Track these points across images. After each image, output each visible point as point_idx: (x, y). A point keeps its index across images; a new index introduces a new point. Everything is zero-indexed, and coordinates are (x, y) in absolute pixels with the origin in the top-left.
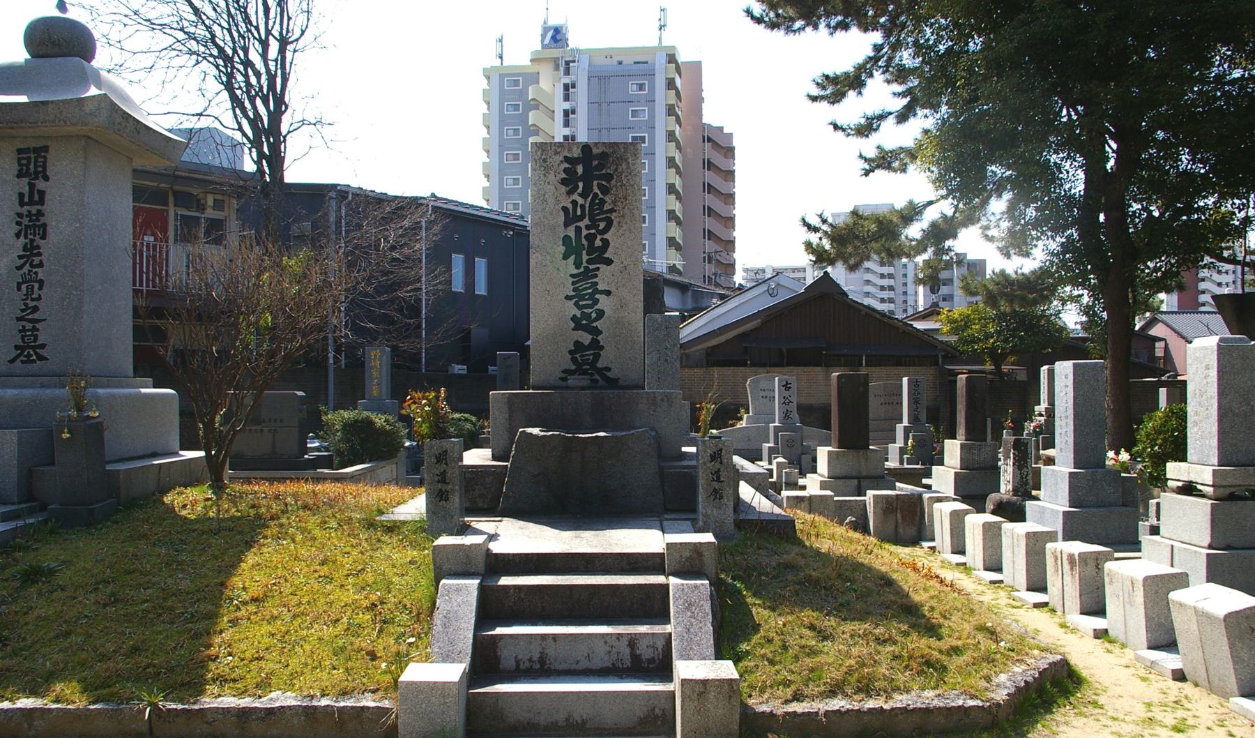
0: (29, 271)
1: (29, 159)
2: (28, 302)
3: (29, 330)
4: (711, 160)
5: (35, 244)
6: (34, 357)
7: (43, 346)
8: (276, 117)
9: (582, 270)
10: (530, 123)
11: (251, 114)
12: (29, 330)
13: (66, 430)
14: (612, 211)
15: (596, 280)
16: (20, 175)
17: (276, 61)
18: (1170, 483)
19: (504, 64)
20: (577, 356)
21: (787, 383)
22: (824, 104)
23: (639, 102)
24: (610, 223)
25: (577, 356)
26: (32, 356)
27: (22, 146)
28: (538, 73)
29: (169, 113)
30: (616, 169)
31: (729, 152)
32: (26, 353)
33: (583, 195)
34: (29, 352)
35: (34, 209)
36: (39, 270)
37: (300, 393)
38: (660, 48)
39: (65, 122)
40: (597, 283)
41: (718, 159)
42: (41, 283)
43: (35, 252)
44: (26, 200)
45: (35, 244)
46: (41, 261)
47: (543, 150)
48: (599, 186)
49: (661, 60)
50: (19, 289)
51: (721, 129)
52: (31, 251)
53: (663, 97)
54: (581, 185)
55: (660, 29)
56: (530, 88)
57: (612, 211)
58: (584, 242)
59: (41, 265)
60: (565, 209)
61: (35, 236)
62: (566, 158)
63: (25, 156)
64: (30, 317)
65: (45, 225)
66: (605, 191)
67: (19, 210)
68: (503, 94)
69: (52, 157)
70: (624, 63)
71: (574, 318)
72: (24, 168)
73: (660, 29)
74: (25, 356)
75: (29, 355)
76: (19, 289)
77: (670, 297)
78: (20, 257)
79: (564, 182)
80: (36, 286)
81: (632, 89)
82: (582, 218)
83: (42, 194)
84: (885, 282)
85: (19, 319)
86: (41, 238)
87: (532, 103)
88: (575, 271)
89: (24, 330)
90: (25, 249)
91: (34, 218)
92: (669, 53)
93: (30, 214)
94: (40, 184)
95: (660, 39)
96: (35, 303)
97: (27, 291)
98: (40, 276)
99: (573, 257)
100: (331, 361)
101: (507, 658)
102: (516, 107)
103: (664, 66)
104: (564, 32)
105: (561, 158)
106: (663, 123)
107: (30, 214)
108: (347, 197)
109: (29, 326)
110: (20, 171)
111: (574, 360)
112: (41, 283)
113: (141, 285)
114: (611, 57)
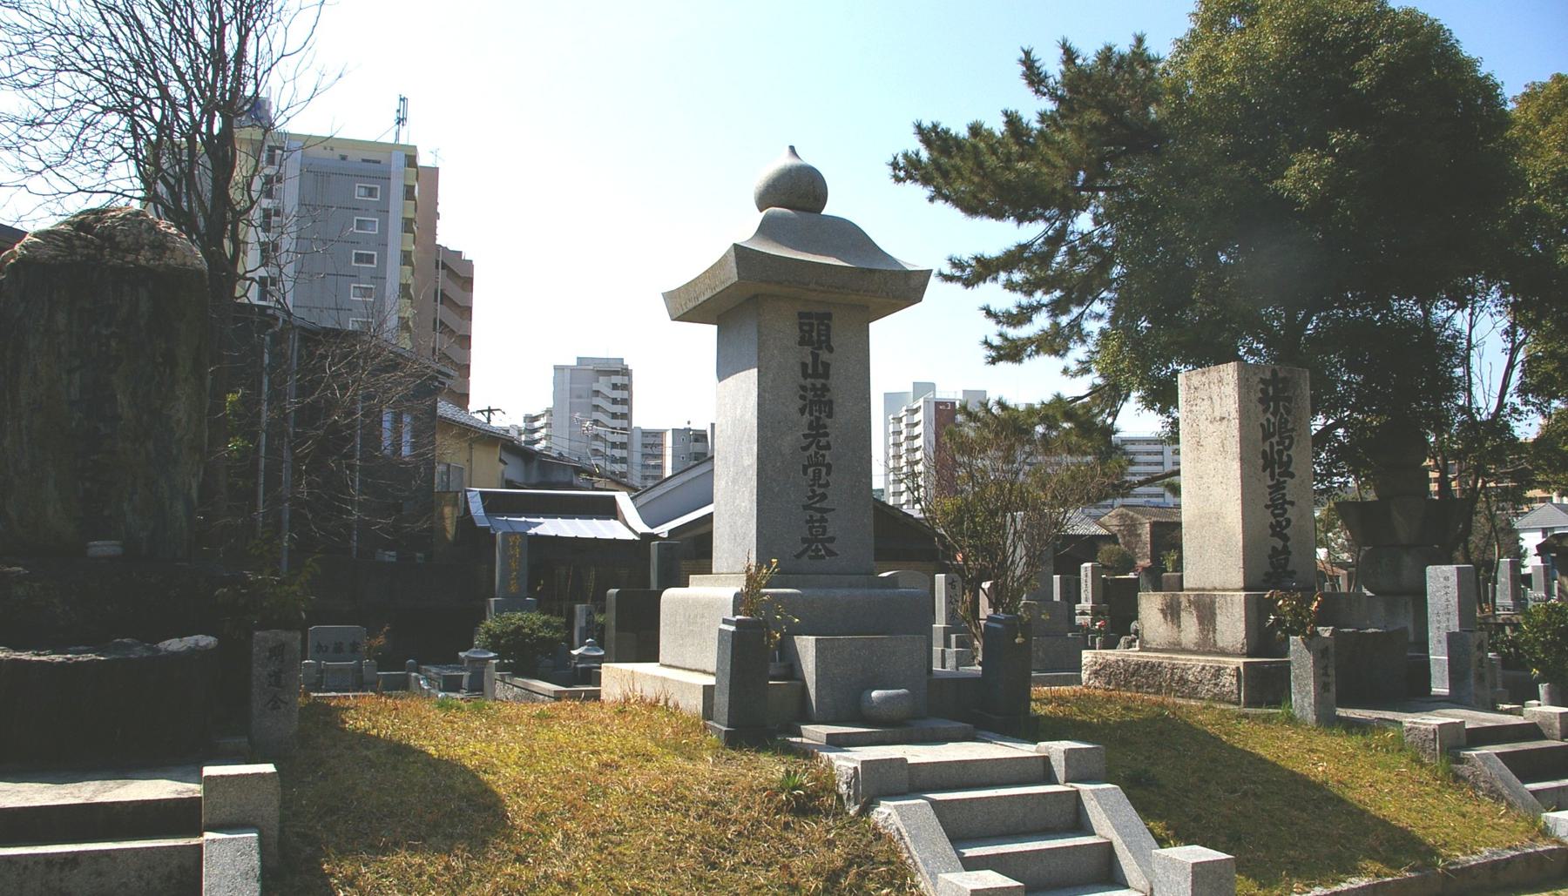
0: (816, 453)
1: (811, 325)
2: (815, 488)
3: (816, 521)
4: (447, 293)
5: (821, 423)
6: (823, 552)
7: (832, 540)
9: (1275, 482)
12: (816, 521)
13: (1019, 635)
14: (1293, 430)
15: (1284, 491)
16: (802, 343)
20: (1274, 560)
21: (954, 581)
22: (958, 286)
23: (367, 210)
25: (1274, 560)
26: (820, 550)
27: (806, 310)
30: (1294, 393)
31: (467, 283)
32: (813, 547)
34: (817, 546)
35: (819, 383)
36: (827, 453)
38: (395, 147)
39: (887, 293)
40: (1284, 495)
41: (454, 291)
42: (829, 467)
43: (821, 431)
44: (810, 371)
45: (821, 423)
46: (828, 442)
47: (1246, 370)
48: (1285, 407)
49: (398, 162)
50: (805, 473)
52: (817, 431)
53: (398, 208)
54: (1272, 404)
57: (1293, 430)
58: (1276, 457)
59: (828, 447)
60: (1262, 425)
61: (820, 413)
62: (1261, 379)
63: (807, 321)
64: (818, 505)
65: (831, 402)
66: (1288, 412)
67: (802, 381)
70: (349, 159)
72: (807, 335)
73: (399, 123)
74: (813, 551)
75: (818, 550)
76: (805, 473)
78: (805, 436)
79: (1261, 401)
80: (824, 470)
81: (359, 193)
82: (1273, 435)
83: (827, 366)
84: (618, 453)
85: (806, 507)
86: (827, 416)
88: (1271, 483)
89: (811, 521)
90: (810, 427)
91: (819, 392)
93: (814, 388)
94: (824, 356)
95: (397, 134)
96: (822, 490)
97: (814, 476)
98: (828, 460)
99: (1269, 470)
103: (402, 170)
104: (267, 108)
105: (1258, 380)
106: (397, 242)
107: (814, 388)
109: (817, 516)
110: (802, 338)
111: (1272, 563)
112: (829, 467)
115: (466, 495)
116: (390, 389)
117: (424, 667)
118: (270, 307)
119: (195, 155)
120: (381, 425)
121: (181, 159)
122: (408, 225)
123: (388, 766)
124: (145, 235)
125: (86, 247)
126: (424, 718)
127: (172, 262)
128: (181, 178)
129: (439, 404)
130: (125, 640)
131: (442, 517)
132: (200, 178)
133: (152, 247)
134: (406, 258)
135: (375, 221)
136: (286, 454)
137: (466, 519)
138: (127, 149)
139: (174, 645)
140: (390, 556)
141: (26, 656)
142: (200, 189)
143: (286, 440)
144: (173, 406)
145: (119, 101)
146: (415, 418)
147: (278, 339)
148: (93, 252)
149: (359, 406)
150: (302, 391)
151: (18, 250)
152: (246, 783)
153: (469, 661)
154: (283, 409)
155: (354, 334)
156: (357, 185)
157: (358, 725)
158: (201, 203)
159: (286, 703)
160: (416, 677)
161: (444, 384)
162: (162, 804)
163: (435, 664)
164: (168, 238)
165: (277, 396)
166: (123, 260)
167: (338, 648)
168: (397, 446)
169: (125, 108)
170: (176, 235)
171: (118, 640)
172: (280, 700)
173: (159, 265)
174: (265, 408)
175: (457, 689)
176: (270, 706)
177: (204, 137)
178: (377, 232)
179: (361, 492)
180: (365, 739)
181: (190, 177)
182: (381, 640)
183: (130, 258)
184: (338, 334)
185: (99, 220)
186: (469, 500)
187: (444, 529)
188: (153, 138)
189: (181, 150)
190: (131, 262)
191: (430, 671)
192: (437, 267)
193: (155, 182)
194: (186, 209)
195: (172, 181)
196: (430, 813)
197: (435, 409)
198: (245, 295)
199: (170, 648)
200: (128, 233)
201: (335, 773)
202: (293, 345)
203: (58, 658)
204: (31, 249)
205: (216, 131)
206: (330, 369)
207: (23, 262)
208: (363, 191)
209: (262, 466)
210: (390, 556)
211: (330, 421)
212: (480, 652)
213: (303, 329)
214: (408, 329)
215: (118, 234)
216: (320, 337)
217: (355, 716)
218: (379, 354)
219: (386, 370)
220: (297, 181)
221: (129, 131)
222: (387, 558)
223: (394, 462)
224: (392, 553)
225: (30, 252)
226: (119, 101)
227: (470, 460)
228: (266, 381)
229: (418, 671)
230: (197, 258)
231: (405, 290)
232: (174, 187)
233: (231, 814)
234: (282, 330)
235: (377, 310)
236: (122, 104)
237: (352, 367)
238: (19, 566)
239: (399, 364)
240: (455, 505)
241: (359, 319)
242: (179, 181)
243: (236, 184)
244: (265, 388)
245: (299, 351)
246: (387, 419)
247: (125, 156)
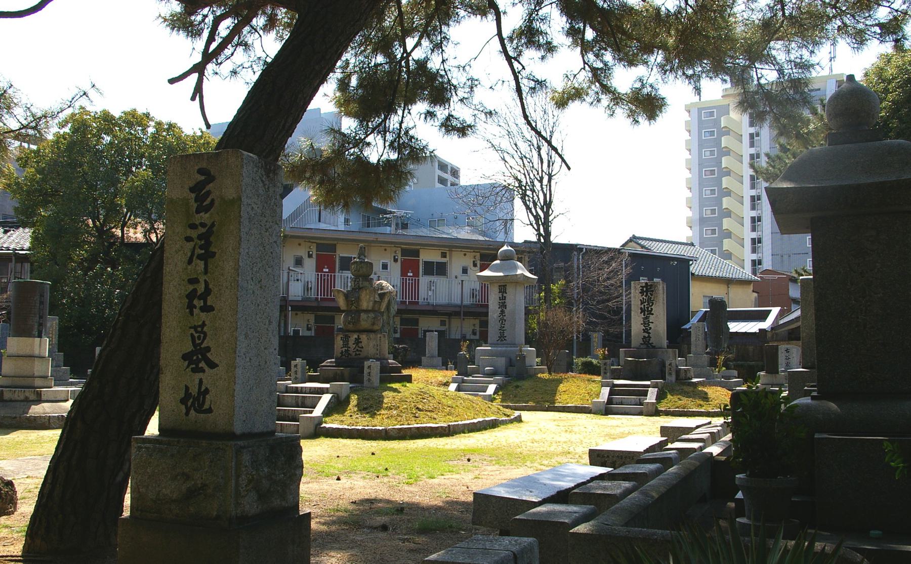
8: (547, 215)
10: (723, 146)
11: (535, 214)
17: (547, 185)
18: (19, 265)
19: (702, 100)
24: (653, 303)
28: (729, 105)
33: (646, 296)
35: (503, 301)
37: (567, 351)
52: (502, 312)
55: (831, 60)
56: (722, 118)
66: (651, 295)
68: (701, 124)
69: (507, 287)
71: (643, 330)
73: (831, 60)
83: (505, 297)
87: (724, 130)
94: (505, 295)
100: (575, 338)
101: (614, 401)
102: (712, 133)
108: (582, 251)
111: (643, 341)
113: (406, 299)
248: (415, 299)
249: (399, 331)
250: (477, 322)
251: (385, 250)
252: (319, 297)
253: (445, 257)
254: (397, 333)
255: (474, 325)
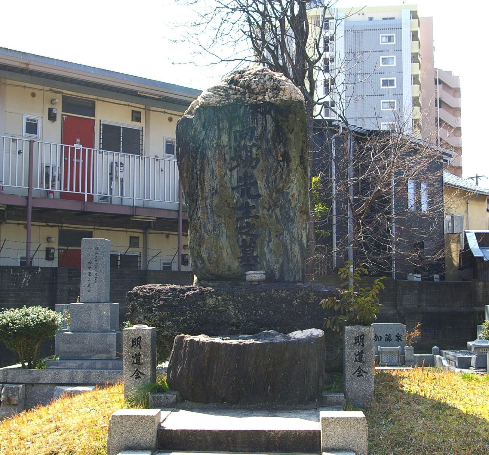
4: (442, 99)
23: (388, 51)
29: (236, 59)
31: (456, 92)
41: (448, 98)
49: (406, 17)
51: (449, 73)
70: (374, 19)
77: (184, 210)
81: (382, 40)
92: (413, 10)
113: (83, 190)
114: (363, 15)
115: (465, 235)
116: (413, 167)
117: (444, 351)
118: (334, 120)
119: (285, 30)
120: (407, 191)
121: (276, 34)
122: (415, 58)
123: (434, 417)
124: (268, 83)
125: (236, 94)
126: (454, 385)
127: (284, 98)
128: (278, 46)
129: (444, 175)
130: (270, 331)
131: (450, 251)
132: (288, 44)
133: (273, 90)
134: (415, 79)
135: (393, 58)
136: (349, 213)
137: (466, 252)
138: (246, 32)
139: (298, 334)
140: (416, 277)
141: (218, 340)
142: (289, 51)
143: (349, 204)
144: (290, 186)
145: (240, 4)
146: (430, 185)
147: (340, 140)
148: (239, 96)
149: (393, 179)
150: (357, 172)
151: (200, 101)
152: (347, 423)
153: (475, 348)
154: (346, 185)
155: (387, 133)
156: (381, 35)
157: (411, 389)
158: (291, 60)
159: (366, 373)
160: (440, 358)
161: (446, 161)
162: (209, 438)
163: (452, 349)
164: (281, 83)
165: (342, 176)
166: (256, 100)
167: (388, 338)
168: (418, 204)
169: (244, 7)
170: (285, 81)
171: (266, 331)
172: (363, 371)
173: (277, 100)
174: (334, 184)
175: (468, 366)
176: (356, 374)
177: (289, 18)
178: (395, 65)
179: (397, 236)
180: (416, 398)
181: (283, 45)
182: (416, 333)
183: (260, 98)
184: (377, 133)
185: (241, 77)
186: (468, 239)
187: (452, 259)
188: (260, 23)
189: (276, 28)
190: (260, 100)
191: (449, 354)
192: (436, 83)
193: (263, 50)
194: (282, 64)
195: (272, 48)
196: (464, 450)
197: (442, 178)
198: (320, 114)
199: (296, 337)
200: (258, 83)
201: (400, 420)
202: (349, 143)
203: (234, 342)
204: (206, 98)
205: (296, 12)
206: (373, 157)
207: (203, 107)
208: (384, 39)
209: (334, 222)
210: (416, 277)
211: (375, 191)
212: (484, 342)
213: (356, 132)
214: (419, 127)
215: (253, 84)
216: (367, 136)
217: (409, 382)
218: (404, 145)
219: (409, 154)
220: (343, 39)
221: (246, 21)
222: (415, 279)
223: (418, 215)
224: (419, 275)
225: (206, 100)
226: (240, 4)
227: (467, 212)
228: (334, 167)
229: (440, 354)
230: (298, 93)
231: (415, 101)
232: (274, 51)
233: (338, 442)
234: (342, 134)
235: (399, 116)
236: (241, 5)
237: (387, 155)
238: (209, 287)
239: (417, 150)
240: (459, 242)
241: (390, 123)
242: (277, 48)
243: (309, 45)
244: (334, 171)
245: (353, 146)
246: (411, 187)
247: (246, 36)
248: (77, 190)
249: (56, 255)
250: (54, 233)
251: (33, 95)
252: (57, 190)
253: (138, 119)
254: (52, 259)
255: (48, 239)
